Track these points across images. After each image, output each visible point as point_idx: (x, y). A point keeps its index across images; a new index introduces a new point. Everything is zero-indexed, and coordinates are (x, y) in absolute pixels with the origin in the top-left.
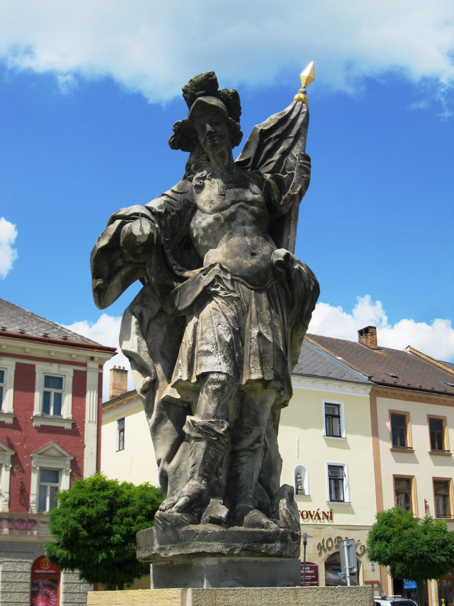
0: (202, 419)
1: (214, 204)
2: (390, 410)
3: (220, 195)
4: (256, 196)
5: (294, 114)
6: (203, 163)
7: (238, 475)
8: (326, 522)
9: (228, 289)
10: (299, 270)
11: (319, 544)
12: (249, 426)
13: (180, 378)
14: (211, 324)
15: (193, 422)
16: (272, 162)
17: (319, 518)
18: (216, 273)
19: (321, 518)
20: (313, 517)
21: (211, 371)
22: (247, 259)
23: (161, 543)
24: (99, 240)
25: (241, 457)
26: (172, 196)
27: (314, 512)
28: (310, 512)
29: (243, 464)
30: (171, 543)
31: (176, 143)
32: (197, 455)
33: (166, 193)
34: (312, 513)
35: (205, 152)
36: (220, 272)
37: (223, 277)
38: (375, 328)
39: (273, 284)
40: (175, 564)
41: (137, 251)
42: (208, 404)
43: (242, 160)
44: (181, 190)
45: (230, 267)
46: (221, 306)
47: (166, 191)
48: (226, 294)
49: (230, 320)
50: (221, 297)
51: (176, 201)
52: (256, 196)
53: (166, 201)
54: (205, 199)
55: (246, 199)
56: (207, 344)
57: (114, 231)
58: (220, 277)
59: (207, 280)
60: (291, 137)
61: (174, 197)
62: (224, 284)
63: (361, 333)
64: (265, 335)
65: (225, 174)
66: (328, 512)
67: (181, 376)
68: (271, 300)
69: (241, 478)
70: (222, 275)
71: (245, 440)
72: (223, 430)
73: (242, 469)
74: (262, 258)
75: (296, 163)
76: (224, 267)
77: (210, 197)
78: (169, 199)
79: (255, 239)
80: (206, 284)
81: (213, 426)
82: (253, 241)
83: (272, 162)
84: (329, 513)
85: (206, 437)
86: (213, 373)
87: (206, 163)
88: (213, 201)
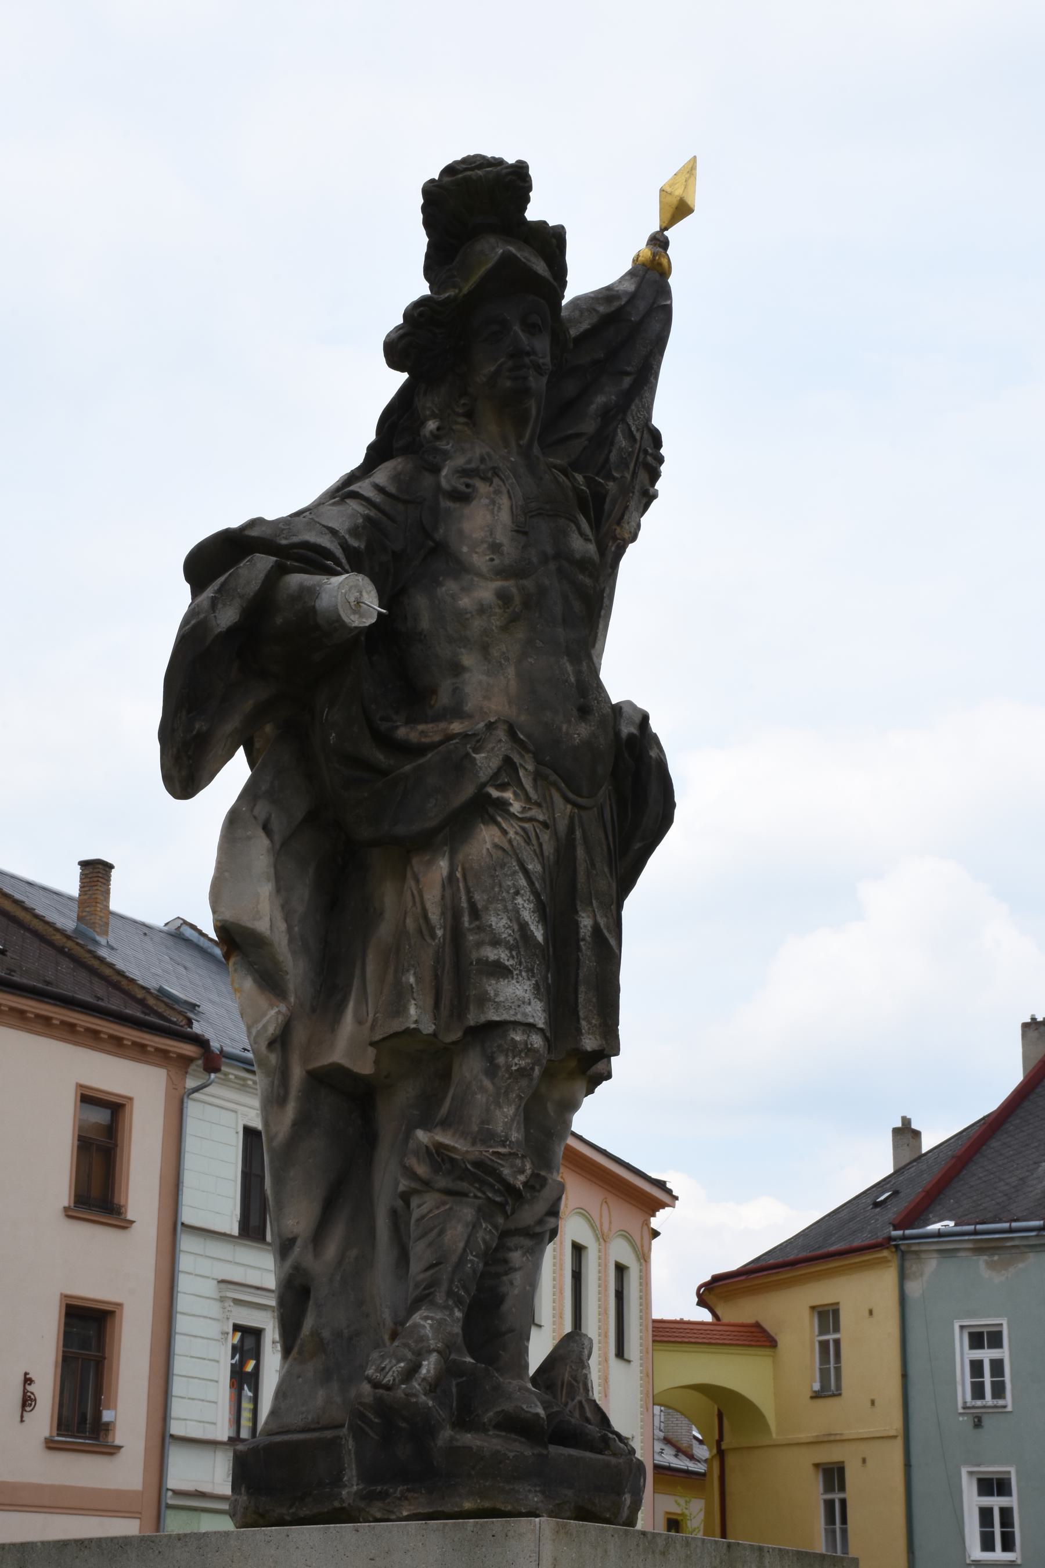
0: (474, 1144)
2: (79, 1086)
3: (517, 531)
6: (457, 423)
7: (500, 1299)
9: (528, 799)
13: (413, 1026)
14: (497, 889)
16: (578, 435)
21: (512, 1019)
22: (569, 722)
25: (510, 1250)
29: (516, 1270)
32: (448, 1237)
42: (492, 1107)
46: (515, 843)
50: (513, 816)
54: (478, 535)
57: (255, 586)
58: (514, 763)
60: (628, 374)
67: (416, 1022)
69: (505, 1307)
70: (516, 759)
71: (526, 1206)
72: (522, 1178)
73: (512, 1284)
75: (633, 452)
78: (373, 513)
81: (503, 1166)
85: (480, 1194)
86: (516, 1024)
87: (466, 424)
88: (500, 545)
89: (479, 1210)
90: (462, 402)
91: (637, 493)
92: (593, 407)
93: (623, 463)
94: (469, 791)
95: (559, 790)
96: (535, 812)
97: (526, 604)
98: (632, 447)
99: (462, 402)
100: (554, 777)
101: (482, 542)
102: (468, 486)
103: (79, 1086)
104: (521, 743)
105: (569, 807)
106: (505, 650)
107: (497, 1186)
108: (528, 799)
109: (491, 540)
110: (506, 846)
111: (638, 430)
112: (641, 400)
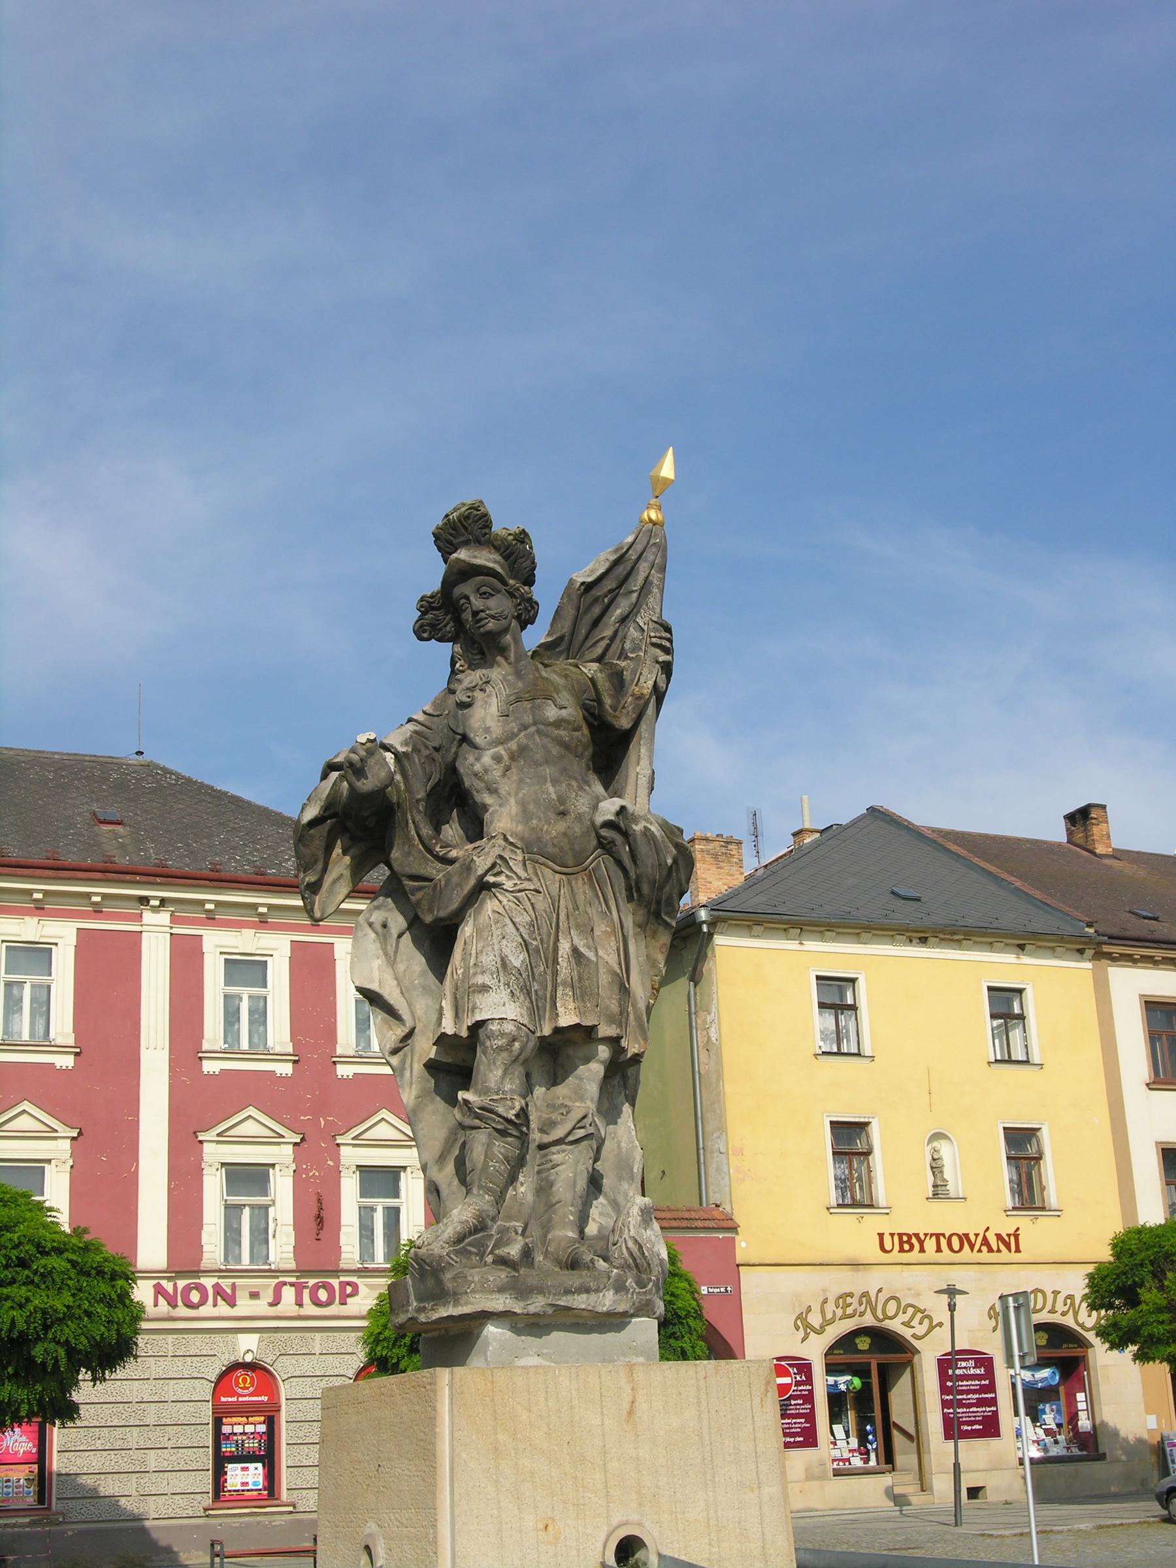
2: (1141, 996)
4: (564, 713)
5: (639, 547)
8: (1005, 1256)
9: (519, 878)
10: (646, 832)
11: (992, 1307)
12: (567, 1102)
15: (466, 1102)
16: (602, 639)
17: (990, 1250)
18: (497, 851)
19: (995, 1248)
20: (977, 1248)
22: (549, 824)
23: (420, 1299)
24: (303, 809)
27: (977, 1235)
28: (966, 1235)
30: (433, 1300)
31: (426, 630)
34: (972, 1238)
38: (1104, 807)
40: (451, 1334)
43: (550, 639)
49: (522, 930)
52: (564, 713)
53: (416, 732)
56: (483, 972)
59: (482, 864)
60: (633, 592)
63: (1071, 818)
64: (582, 950)
66: (977, 1235)
72: (514, 1112)
78: (419, 728)
80: (480, 872)
83: (602, 639)
84: (1012, 1238)
89: (490, 1135)
93: (635, 648)
94: (472, 882)
95: (548, 867)
96: (526, 885)
97: (513, 758)
103: (1141, 996)
104: (511, 844)
107: (497, 1119)
108: (519, 878)
110: (501, 910)
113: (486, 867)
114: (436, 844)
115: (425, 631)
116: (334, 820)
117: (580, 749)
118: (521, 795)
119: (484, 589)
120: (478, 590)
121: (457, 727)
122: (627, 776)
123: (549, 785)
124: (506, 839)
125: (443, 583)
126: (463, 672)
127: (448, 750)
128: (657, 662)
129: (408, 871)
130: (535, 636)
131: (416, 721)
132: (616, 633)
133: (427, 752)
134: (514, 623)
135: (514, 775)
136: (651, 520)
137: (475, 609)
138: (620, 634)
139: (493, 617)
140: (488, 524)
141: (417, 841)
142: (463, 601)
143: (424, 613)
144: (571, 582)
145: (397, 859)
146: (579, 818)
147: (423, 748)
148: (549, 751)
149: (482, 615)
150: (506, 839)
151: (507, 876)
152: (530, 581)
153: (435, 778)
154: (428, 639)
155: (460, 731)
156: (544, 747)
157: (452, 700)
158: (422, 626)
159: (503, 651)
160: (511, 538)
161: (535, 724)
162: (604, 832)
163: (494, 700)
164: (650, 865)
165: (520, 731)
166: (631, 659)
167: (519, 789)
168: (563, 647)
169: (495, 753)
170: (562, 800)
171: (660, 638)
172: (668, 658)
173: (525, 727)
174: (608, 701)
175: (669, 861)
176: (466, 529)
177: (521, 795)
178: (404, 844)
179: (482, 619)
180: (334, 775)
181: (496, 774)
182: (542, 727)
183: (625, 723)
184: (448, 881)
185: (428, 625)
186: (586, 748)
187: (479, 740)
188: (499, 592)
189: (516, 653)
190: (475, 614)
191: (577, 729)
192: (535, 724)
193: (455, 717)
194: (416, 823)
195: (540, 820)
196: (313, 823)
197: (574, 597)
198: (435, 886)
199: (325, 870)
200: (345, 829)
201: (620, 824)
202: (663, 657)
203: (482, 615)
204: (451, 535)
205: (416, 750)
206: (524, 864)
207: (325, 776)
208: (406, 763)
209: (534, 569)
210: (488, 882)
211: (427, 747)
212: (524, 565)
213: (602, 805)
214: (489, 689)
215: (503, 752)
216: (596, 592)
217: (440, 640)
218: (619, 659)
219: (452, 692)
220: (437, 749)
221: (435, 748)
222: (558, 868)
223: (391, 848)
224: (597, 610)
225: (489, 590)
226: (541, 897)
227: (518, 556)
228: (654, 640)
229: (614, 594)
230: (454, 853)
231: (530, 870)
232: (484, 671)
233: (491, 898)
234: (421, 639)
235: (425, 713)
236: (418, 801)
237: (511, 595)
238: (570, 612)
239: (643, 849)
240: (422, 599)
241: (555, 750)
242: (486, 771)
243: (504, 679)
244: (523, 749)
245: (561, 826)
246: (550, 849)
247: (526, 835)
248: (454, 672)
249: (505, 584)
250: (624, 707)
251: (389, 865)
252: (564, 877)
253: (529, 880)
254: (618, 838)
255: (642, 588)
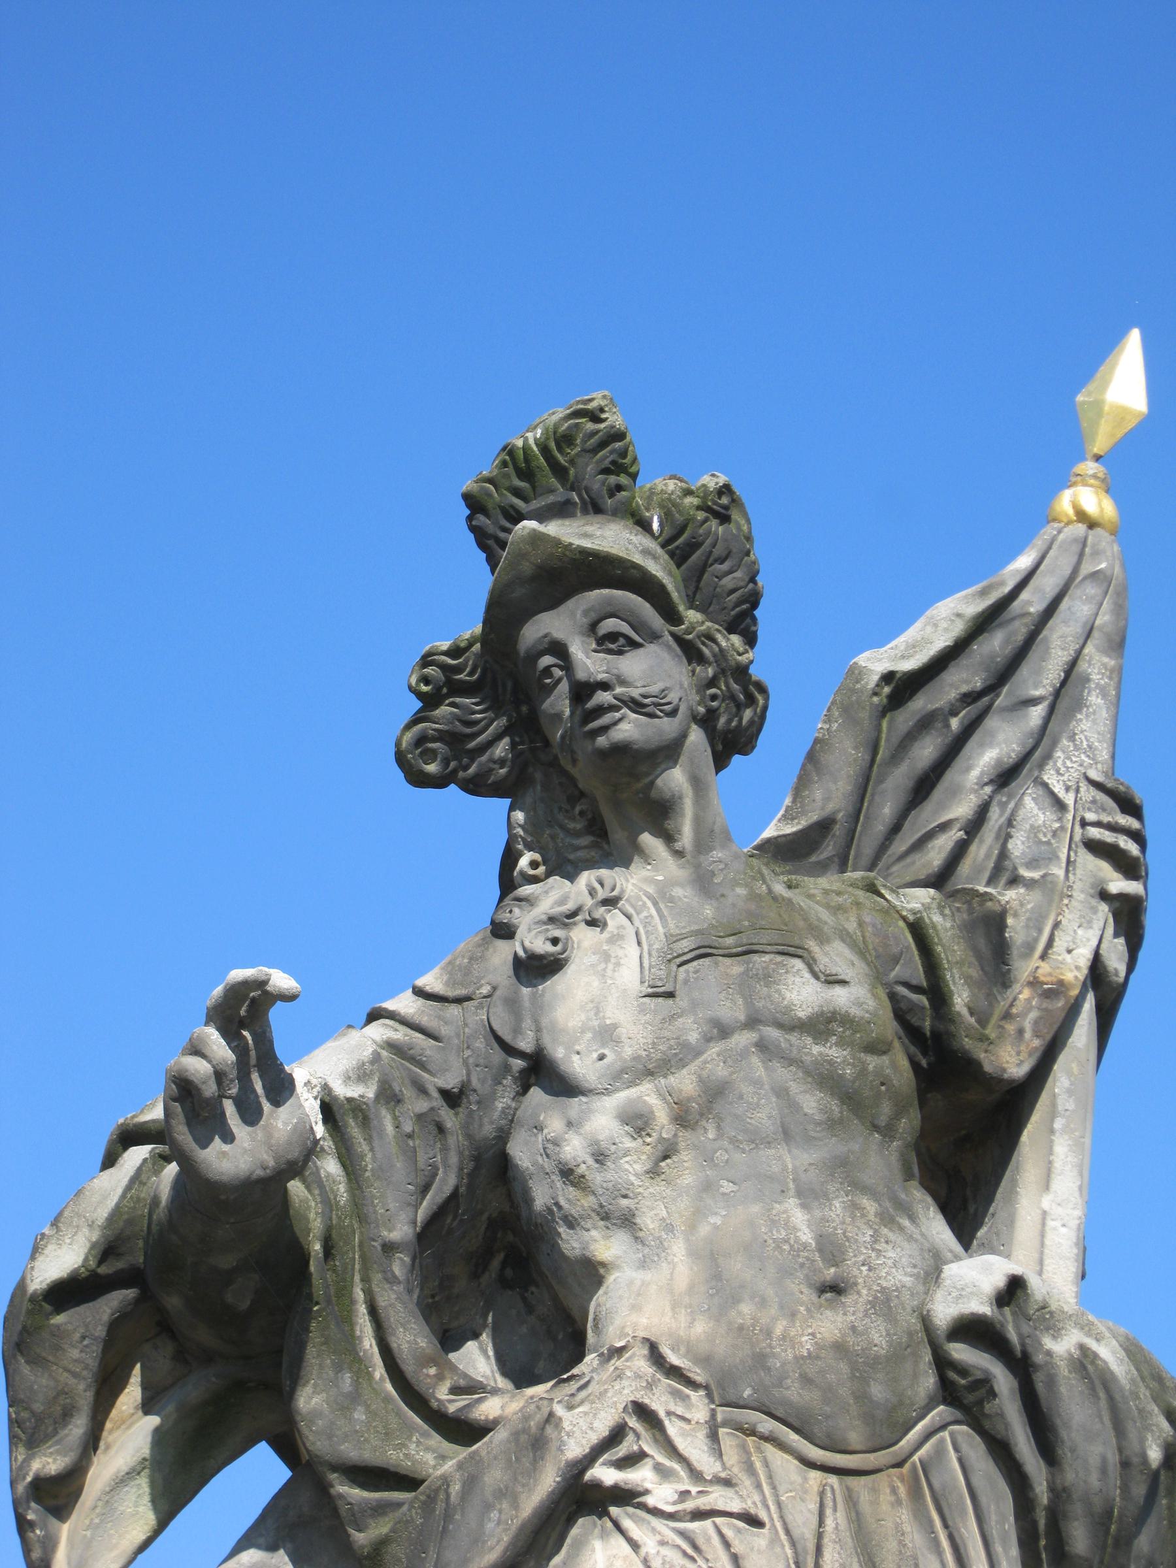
1: (618, 1042)
6: (578, 848)
9: (696, 1475)
10: (1084, 1362)
16: (944, 827)
18: (627, 1392)
24: (36, 1251)
26: (417, 1019)
33: (390, 1005)
35: (582, 794)
36: (650, 1386)
37: (669, 1413)
39: (942, 1440)
41: (229, 1298)
44: (462, 984)
45: (706, 1361)
47: (391, 996)
48: (684, 1495)
50: (656, 1512)
51: (435, 1038)
52: (841, 997)
53: (391, 1046)
55: (788, 1009)
59: (581, 1425)
60: (1034, 701)
61: (425, 1021)
62: (672, 1450)
65: (678, 892)
68: (931, 1522)
70: (659, 1403)
74: (872, 1304)
76: (674, 1359)
77: (598, 1011)
78: (400, 1034)
79: (837, 1208)
80: (575, 1449)
82: (825, 1220)
83: (944, 827)
88: (615, 1026)
90: (578, 809)
91: (1079, 895)
92: (975, 773)
94: (548, 1480)
97: (683, 1118)
98: (1060, 819)
99: (578, 809)
100: (767, 1425)
101: (583, 1032)
102: (555, 941)
104: (674, 1372)
105: (815, 1476)
106: (664, 1213)
108: (696, 1475)
109: (596, 1023)
111: (1068, 789)
112: (1072, 738)
113: (594, 1438)
114: (440, 1377)
115: (429, 756)
116: (130, 1293)
117: (886, 1109)
118: (704, 1230)
119: (610, 625)
120: (593, 627)
121: (517, 1031)
122: (1011, 1223)
123: (792, 1203)
124: (656, 1356)
125: (489, 621)
126: (535, 880)
127: (485, 1103)
128: (1104, 896)
129: (351, 1452)
130: (757, 800)
131: (392, 1015)
132: (982, 812)
133: (422, 1106)
134: (696, 736)
135: (686, 1170)
136: (1082, 516)
137: (581, 675)
138: (996, 817)
139: (636, 706)
140: (622, 466)
141: (379, 1371)
142: (547, 660)
143: (430, 701)
144: (856, 674)
145: (316, 1414)
146: (883, 1304)
147: (408, 1093)
148: (793, 1106)
149: (603, 697)
150: (656, 1356)
151: (658, 1468)
152: (743, 623)
153: (446, 1183)
154: (439, 782)
155: (525, 1044)
156: (781, 1093)
157: (502, 953)
158: (421, 740)
159: (659, 814)
160: (689, 500)
161: (752, 1022)
162: (960, 1352)
163: (630, 953)
164: (1094, 1461)
165: (708, 1039)
166: (1031, 884)
167: (699, 1214)
168: (828, 849)
169: (630, 1102)
170: (831, 1248)
171: (1113, 828)
172: (1132, 887)
173: (723, 1031)
174: (960, 999)
175: (1155, 1455)
176: (559, 471)
177: (704, 1230)
178: (338, 1368)
179: (601, 710)
180: (137, 1155)
181: (632, 1165)
182: (772, 1033)
183: (1012, 1061)
184: (471, 1483)
185: (441, 736)
186: (900, 1111)
187: (580, 1065)
188: (654, 637)
189: (698, 821)
190: (582, 691)
191: (875, 1048)
192: (752, 1022)
193: (512, 1003)
194: (378, 1307)
195: (763, 1303)
196: (68, 1292)
197: (864, 715)
198: (431, 1499)
199: (92, 1442)
200: (165, 1327)
201: (1003, 1332)
202: (1119, 884)
203: (603, 697)
204: (517, 493)
205: (388, 1096)
206: (713, 1436)
207: (110, 1161)
208: (354, 1129)
209: (755, 605)
210: (597, 1485)
211: (422, 1090)
212: (728, 582)
213: (952, 1271)
214: (614, 919)
215: (653, 1101)
216: (920, 704)
217: (475, 787)
218: (989, 882)
219: (502, 931)
220: (452, 1098)
221: (445, 1094)
222: (815, 1453)
223: (295, 1380)
224: (926, 751)
225: (625, 628)
226: (760, 1539)
227: (708, 574)
228: (1094, 833)
229: (979, 705)
230: (490, 1408)
231: (732, 1456)
232: (603, 872)
233: (604, 1535)
234: (418, 779)
235: (419, 992)
236: (389, 1248)
237: (690, 651)
238: (846, 758)
239: (1076, 1412)
240: (426, 660)
241: (811, 1102)
242: (600, 1157)
243: (662, 897)
244: (715, 1093)
245: (830, 1324)
246: (794, 1393)
247: (722, 1348)
248: (508, 882)
249: (671, 615)
250: (1007, 1016)
251: (288, 1447)
252: (833, 1480)
253: (727, 1483)
254: (1003, 1380)
255: (1057, 694)
